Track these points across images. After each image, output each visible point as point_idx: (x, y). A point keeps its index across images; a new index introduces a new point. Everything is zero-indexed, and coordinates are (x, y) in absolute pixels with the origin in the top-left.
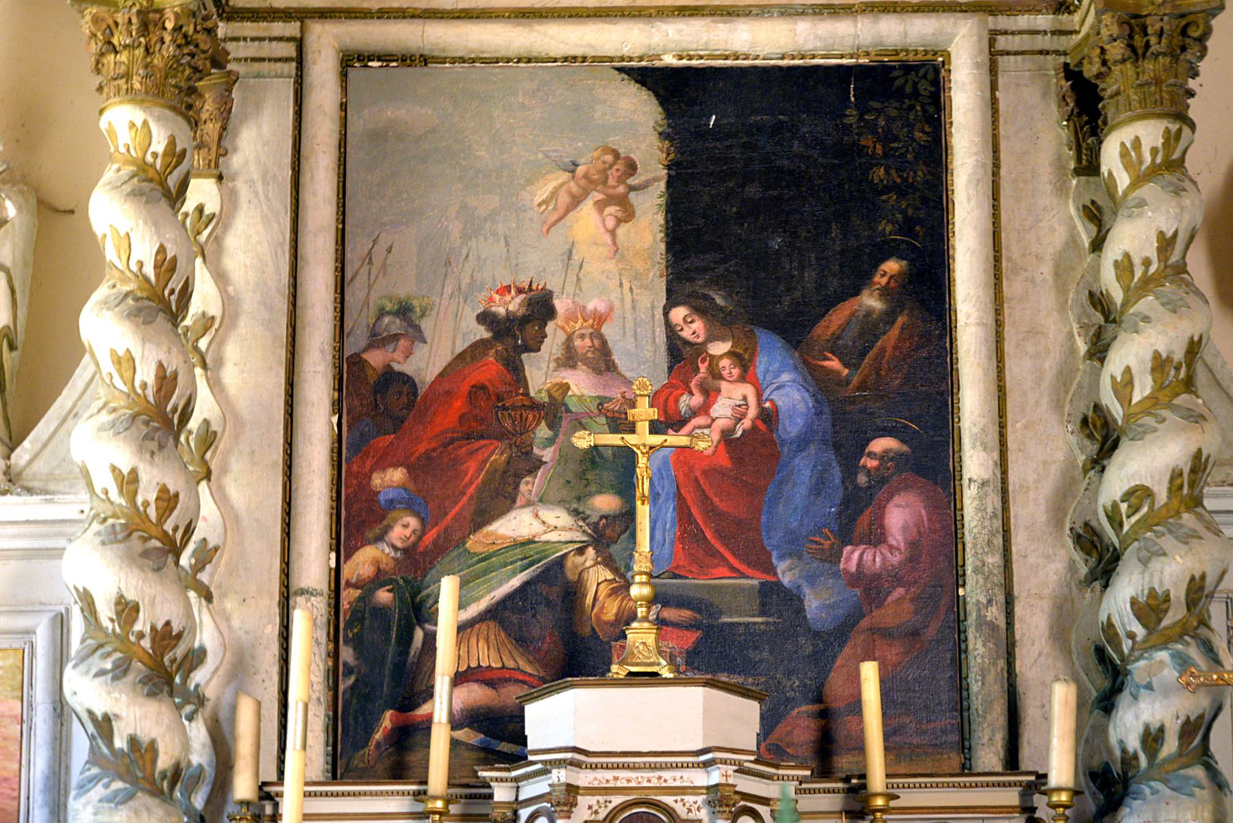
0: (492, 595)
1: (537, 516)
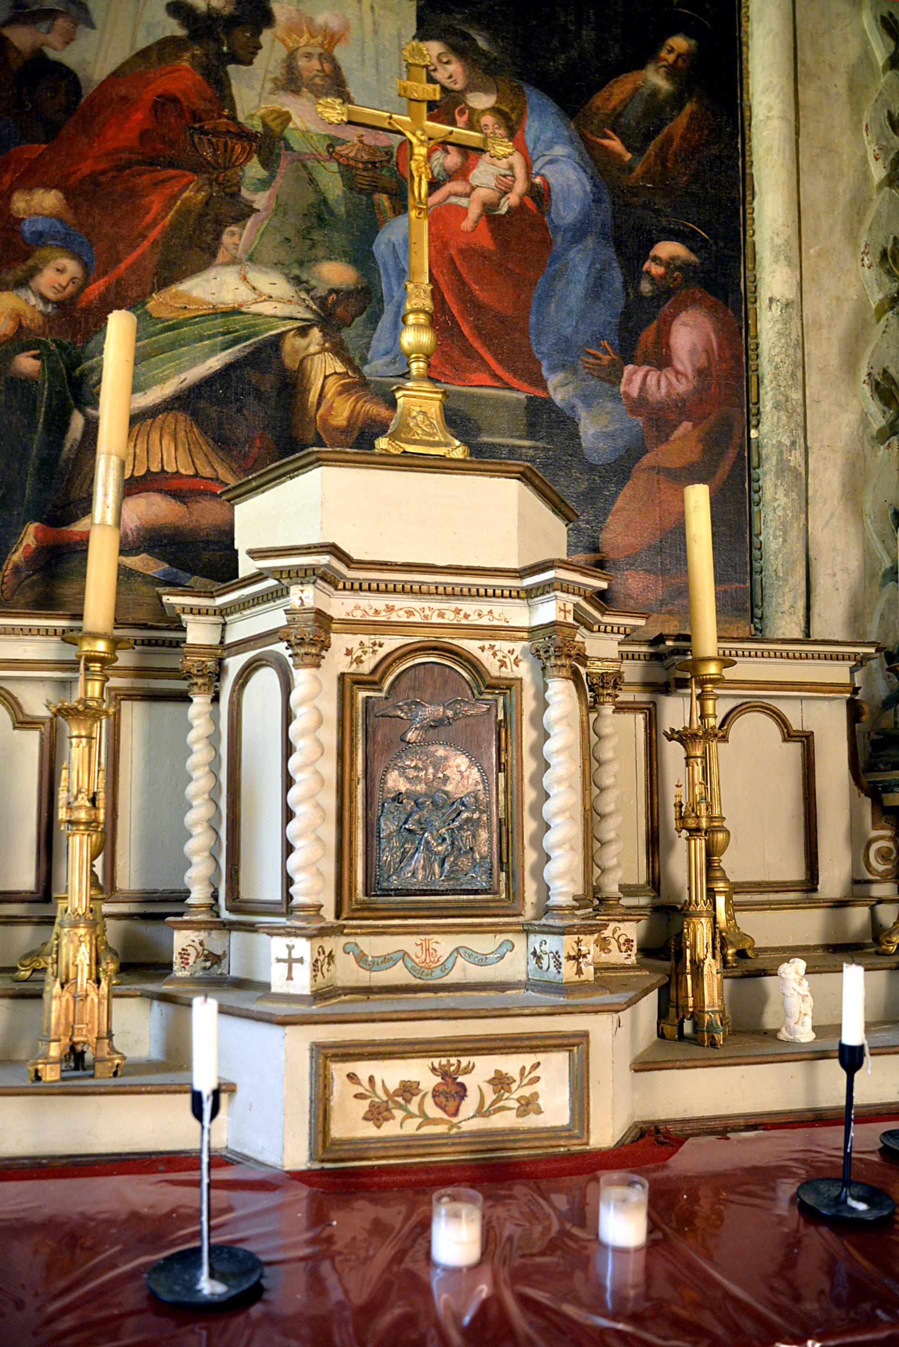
0: (183, 376)
1: (245, 279)
